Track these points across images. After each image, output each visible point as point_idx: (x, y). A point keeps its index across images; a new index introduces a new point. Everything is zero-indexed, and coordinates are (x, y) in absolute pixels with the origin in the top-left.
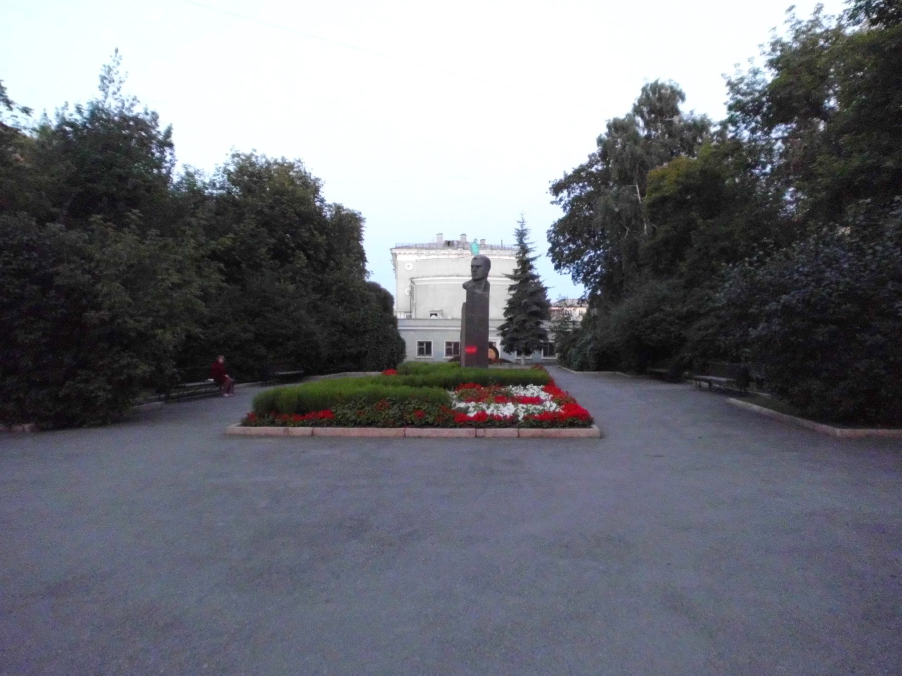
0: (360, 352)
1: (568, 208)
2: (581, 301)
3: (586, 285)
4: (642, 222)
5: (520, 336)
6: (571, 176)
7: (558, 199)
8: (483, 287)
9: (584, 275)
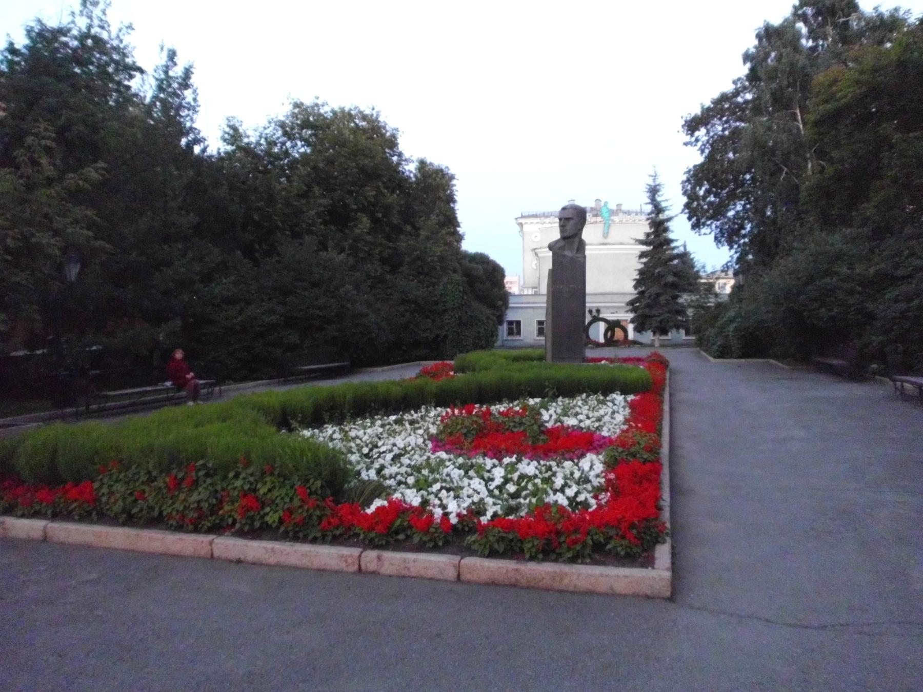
0: (438, 336)
1: (707, 151)
2: (725, 269)
3: (731, 248)
4: (806, 160)
5: (654, 312)
6: (709, 109)
7: (693, 139)
8: (576, 246)
9: (728, 236)
